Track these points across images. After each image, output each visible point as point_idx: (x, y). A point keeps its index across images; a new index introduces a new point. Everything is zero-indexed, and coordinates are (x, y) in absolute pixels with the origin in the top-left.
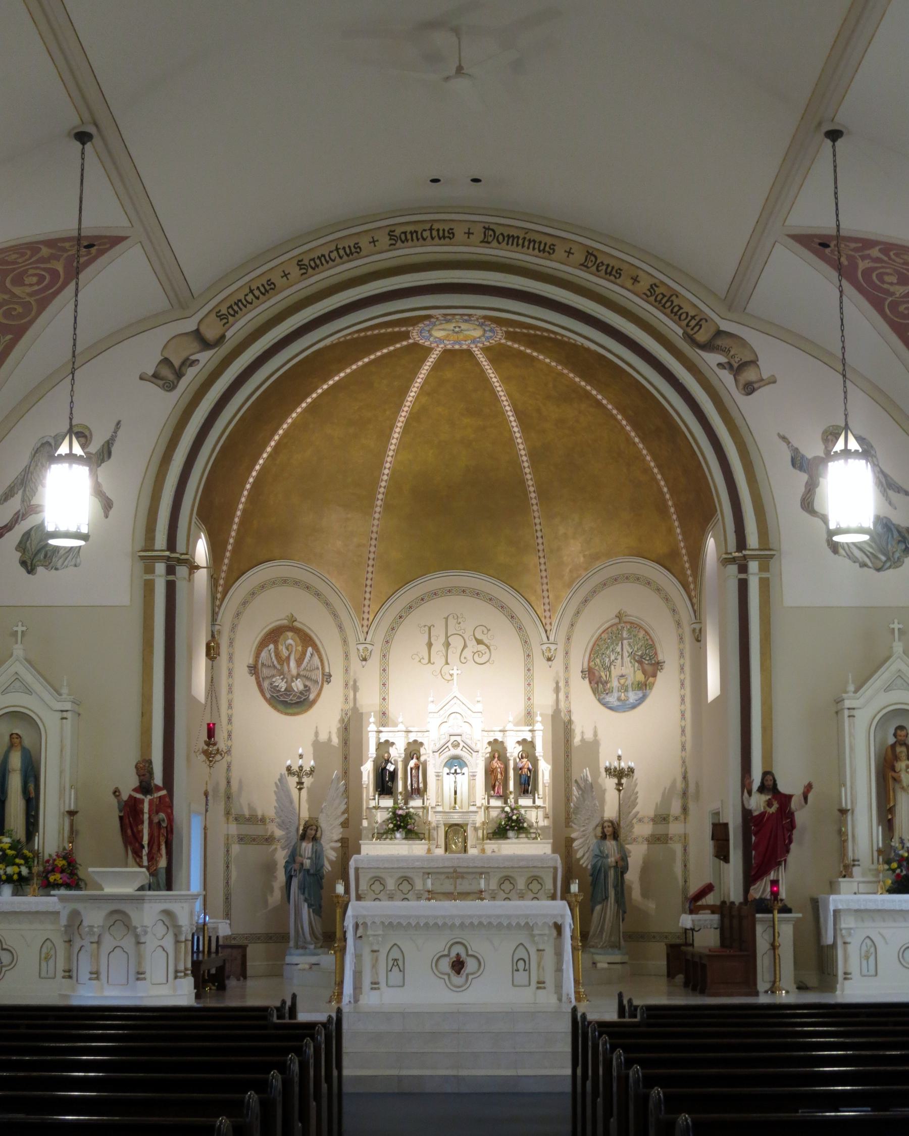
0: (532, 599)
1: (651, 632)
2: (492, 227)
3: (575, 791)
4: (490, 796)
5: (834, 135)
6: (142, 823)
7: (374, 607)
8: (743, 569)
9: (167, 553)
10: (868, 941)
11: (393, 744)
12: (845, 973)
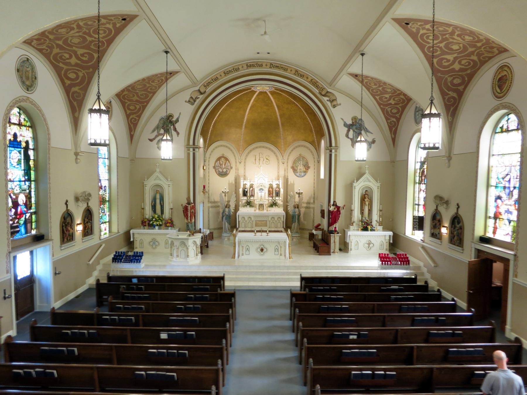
0: (280, 149)
1: (307, 159)
2: (272, 63)
3: (289, 197)
5: (363, 55)
8: (331, 151)
9: (193, 146)
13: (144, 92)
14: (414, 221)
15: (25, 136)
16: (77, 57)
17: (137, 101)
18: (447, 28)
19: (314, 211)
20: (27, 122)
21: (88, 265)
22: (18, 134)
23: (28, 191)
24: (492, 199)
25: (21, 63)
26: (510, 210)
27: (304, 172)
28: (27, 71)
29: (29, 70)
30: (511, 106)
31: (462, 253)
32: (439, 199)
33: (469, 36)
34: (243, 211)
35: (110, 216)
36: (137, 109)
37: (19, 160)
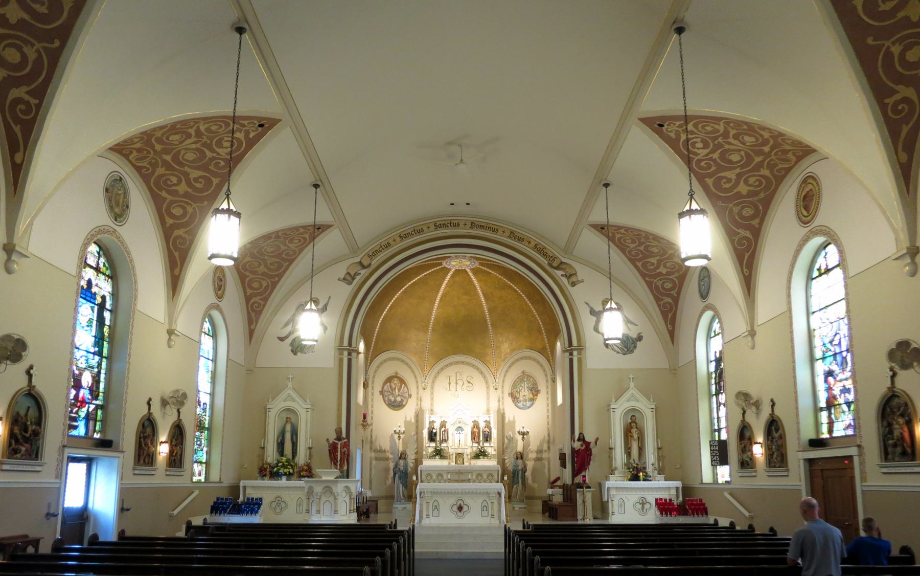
0: (490, 366)
3: (506, 441)
4: (473, 442)
5: (606, 185)
6: (338, 452)
7: (429, 369)
8: (571, 354)
9: (348, 347)
10: (621, 500)
11: (435, 422)
12: (613, 513)
13: (276, 260)
14: (711, 450)
15: (102, 288)
16: (189, 184)
17: (264, 274)
18: (716, 126)
19: (549, 464)
20: (107, 269)
21: (171, 516)
22: (94, 283)
23: (96, 370)
24: (820, 380)
25: (113, 181)
26: (847, 387)
27: (531, 401)
28: (118, 194)
29: (121, 194)
30: (823, 228)
31: (787, 476)
32: (743, 398)
33: (750, 136)
34: (427, 463)
35: (209, 453)
36: (263, 287)
37: (90, 320)
